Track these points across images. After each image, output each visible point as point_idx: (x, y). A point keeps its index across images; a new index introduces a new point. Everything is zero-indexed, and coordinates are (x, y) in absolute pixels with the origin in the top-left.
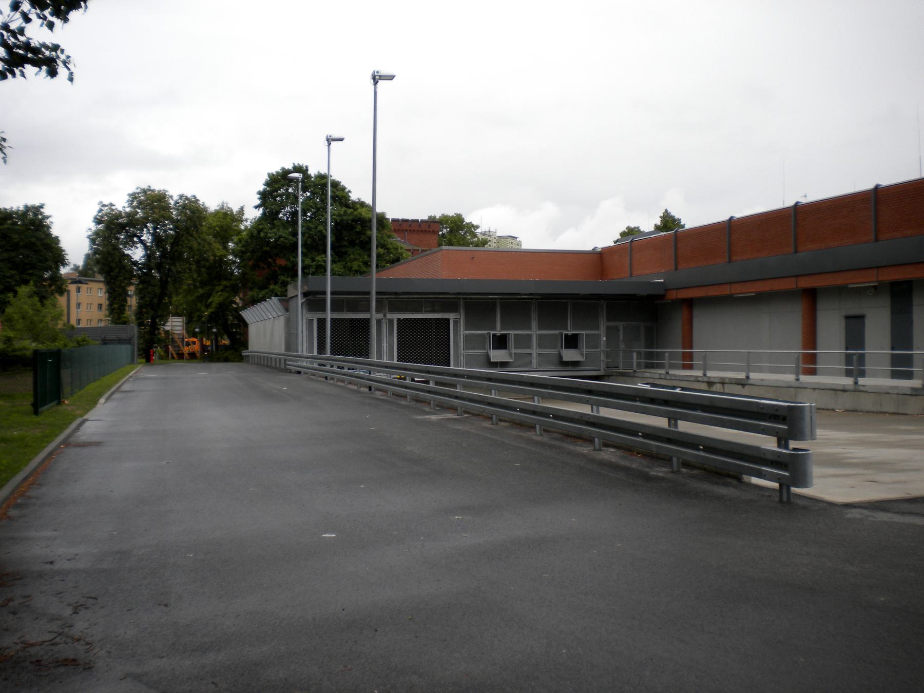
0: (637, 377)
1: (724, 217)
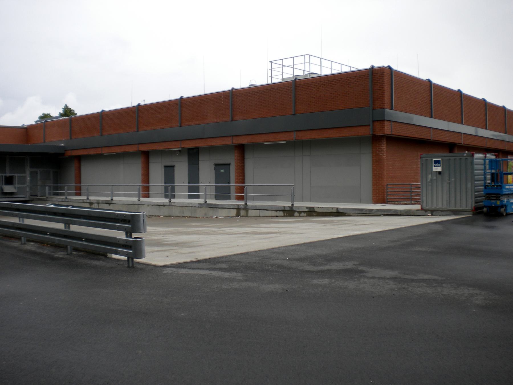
0: (48, 201)
1: (99, 110)
